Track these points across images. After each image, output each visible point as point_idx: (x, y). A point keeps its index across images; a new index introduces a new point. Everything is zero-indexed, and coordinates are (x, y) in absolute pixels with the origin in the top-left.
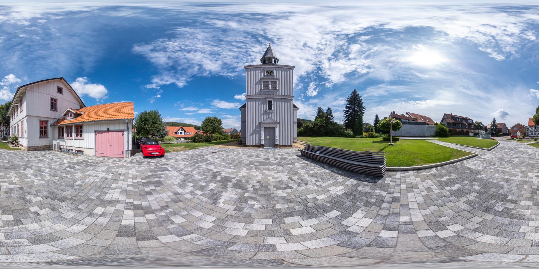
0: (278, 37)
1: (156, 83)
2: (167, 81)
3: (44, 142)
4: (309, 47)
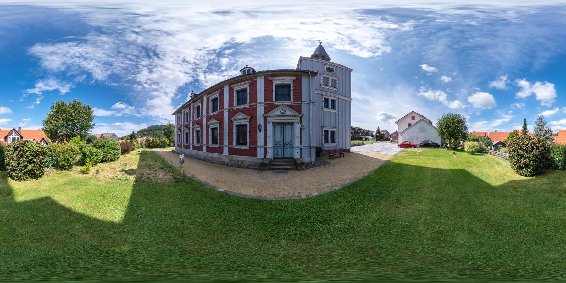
0: (163, 53)
1: (40, 88)
2: (52, 87)
4: (187, 62)
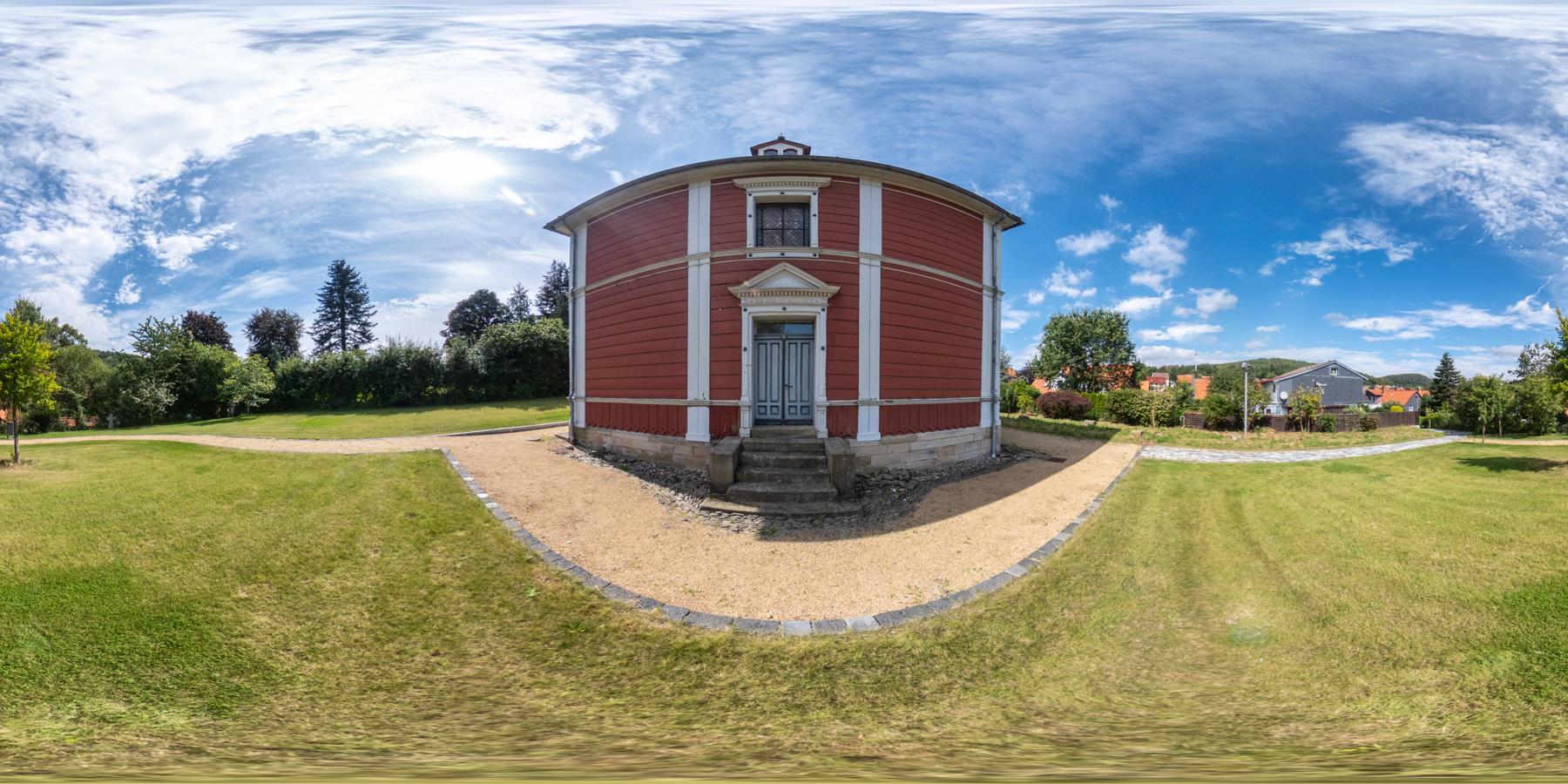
1: (1335, 241)
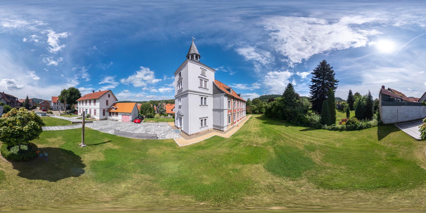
3: (104, 117)
